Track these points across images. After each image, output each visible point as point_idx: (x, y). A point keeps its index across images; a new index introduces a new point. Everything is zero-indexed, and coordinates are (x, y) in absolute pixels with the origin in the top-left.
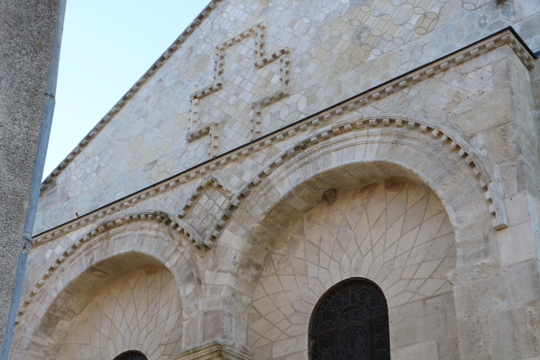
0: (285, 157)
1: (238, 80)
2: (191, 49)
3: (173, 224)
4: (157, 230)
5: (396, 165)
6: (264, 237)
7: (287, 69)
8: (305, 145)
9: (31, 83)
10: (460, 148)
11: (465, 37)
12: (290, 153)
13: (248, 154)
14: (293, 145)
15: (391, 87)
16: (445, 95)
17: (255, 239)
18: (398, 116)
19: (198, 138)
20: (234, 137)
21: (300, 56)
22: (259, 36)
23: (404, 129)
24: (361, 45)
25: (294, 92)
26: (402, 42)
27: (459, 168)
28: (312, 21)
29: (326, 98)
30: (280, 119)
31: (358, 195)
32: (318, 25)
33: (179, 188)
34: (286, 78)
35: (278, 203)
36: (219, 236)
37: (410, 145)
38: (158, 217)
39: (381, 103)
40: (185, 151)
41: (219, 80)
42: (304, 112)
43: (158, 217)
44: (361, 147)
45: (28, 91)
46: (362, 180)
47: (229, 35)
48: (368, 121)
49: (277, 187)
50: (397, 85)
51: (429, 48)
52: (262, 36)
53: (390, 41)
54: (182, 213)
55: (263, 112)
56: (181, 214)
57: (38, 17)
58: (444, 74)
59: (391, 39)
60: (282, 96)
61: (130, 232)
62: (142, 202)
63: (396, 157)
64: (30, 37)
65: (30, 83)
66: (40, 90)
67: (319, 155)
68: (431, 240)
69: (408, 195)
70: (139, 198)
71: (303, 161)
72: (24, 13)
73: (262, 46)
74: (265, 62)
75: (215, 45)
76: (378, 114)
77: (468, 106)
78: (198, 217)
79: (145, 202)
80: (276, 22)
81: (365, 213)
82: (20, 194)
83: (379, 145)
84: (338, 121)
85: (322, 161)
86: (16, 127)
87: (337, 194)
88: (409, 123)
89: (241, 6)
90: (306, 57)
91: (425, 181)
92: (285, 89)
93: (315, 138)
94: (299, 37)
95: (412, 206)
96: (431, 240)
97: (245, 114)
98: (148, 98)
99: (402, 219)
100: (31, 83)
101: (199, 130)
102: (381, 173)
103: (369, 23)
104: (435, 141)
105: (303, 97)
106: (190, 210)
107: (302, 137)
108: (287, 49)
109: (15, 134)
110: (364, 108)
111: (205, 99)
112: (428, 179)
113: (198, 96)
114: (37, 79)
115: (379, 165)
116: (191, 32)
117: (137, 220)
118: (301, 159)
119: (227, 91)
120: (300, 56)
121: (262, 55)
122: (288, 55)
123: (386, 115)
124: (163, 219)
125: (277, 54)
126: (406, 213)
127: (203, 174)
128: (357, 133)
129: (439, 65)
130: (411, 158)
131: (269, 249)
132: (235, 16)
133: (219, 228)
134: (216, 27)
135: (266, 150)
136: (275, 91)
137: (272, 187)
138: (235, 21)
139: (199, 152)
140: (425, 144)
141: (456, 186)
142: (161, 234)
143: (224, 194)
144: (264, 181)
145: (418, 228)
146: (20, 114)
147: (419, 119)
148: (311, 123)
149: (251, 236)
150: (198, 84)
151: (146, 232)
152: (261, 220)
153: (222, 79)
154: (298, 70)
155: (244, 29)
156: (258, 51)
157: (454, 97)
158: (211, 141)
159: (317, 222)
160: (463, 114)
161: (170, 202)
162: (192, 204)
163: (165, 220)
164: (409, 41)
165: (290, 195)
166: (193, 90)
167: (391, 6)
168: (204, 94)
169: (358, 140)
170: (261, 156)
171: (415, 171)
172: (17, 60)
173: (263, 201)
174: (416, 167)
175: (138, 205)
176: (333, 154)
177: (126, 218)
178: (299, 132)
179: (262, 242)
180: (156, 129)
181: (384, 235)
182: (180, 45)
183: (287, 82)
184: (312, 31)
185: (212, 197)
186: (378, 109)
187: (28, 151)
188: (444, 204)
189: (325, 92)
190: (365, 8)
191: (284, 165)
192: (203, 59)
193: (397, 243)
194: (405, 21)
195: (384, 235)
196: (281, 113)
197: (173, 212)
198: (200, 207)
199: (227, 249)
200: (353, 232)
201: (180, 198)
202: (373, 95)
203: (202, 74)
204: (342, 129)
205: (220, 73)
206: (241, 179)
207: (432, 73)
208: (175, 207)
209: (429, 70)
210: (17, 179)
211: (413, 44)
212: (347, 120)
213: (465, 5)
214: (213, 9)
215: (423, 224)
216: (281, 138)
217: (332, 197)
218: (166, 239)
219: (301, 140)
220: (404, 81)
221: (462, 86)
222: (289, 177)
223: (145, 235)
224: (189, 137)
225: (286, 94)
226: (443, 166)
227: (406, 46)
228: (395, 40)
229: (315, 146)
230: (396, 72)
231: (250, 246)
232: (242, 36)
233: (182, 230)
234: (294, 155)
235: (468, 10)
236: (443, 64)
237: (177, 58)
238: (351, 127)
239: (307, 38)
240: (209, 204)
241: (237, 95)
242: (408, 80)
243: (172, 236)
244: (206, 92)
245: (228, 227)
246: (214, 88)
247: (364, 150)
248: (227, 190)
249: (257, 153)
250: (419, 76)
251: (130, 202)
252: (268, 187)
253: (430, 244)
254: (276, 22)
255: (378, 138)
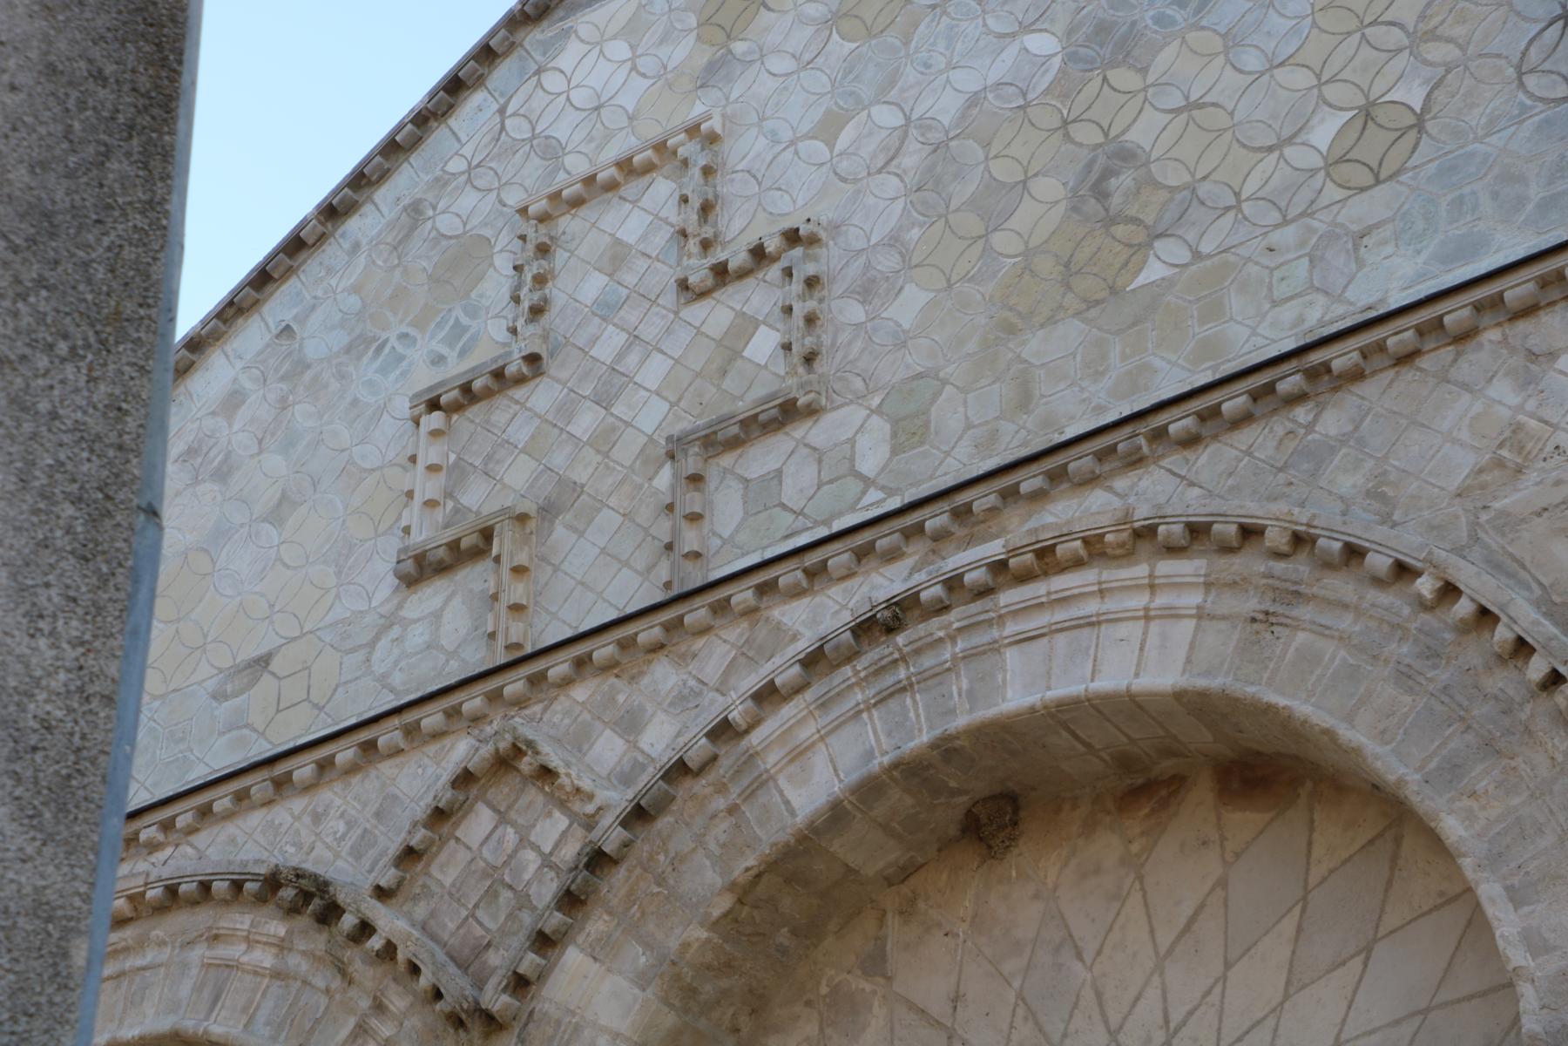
0: (815, 661)
1: (609, 344)
2: (415, 211)
3: (348, 921)
4: (282, 946)
5: (1269, 709)
6: (724, 983)
7: (811, 304)
8: (896, 617)
9: (90, 468)
10: (1533, 650)
11: (1530, 207)
12: (837, 648)
13: (662, 646)
14: (846, 617)
15: (1243, 398)
16: (1464, 435)
17: (690, 992)
18: (1277, 515)
19: (442, 569)
20: (598, 574)
21: (862, 260)
22: (696, 172)
23: (1299, 568)
24: (1110, 221)
25: (839, 400)
26: (1275, 217)
27: (1528, 731)
28: (908, 119)
29: (969, 426)
30: (783, 506)
31: (1108, 819)
32: (936, 136)
33: (373, 773)
34: (809, 341)
35: (787, 845)
36: (542, 976)
37: (1323, 631)
38: (288, 893)
39: (1204, 458)
40: (390, 621)
41: (530, 340)
42: (881, 481)
43: (288, 893)
44: (1123, 630)
45: (80, 499)
46: (1125, 762)
47: (569, 161)
48: (1151, 531)
49: (782, 782)
50: (1270, 389)
51: (1385, 242)
52: (707, 171)
53: (1228, 209)
54: (388, 878)
55: (713, 473)
56: (383, 883)
57: (109, 207)
58: (1458, 355)
59: (1232, 201)
60: (788, 413)
61: (165, 954)
62: (215, 829)
63: (1266, 675)
64: (81, 287)
65: (85, 468)
66: (121, 496)
67: (954, 657)
68: (1413, 1015)
69: (1312, 829)
70: (205, 812)
71: (888, 680)
72: (60, 195)
73: (706, 209)
74: (721, 273)
75: (514, 198)
76: (1193, 504)
77: (1558, 483)
78: (455, 895)
79: (230, 829)
80: (762, 119)
81: (1136, 897)
82: (60, 913)
83: (1197, 628)
84: (1031, 524)
85: (965, 684)
86: (42, 643)
87: (1022, 814)
88: (1321, 542)
89: (619, 50)
90: (887, 262)
91: (1391, 778)
92: (801, 386)
93: (937, 591)
94: (855, 181)
95: (1331, 871)
96: (1413, 1015)
97: (638, 480)
98: (233, 401)
99: (1288, 925)
100: (90, 468)
101: (448, 535)
102: (1199, 737)
103: (1139, 136)
104: (1425, 617)
105: (875, 419)
106: (419, 867)
107: (884, 584)
108: (811, 227)
109: (38, 673)
110: (1133, 475)
111: (475, 411)
112: (1402, 770)
113: (443, 400)
114: (111, 453)
115: (1196, 704)
116: (415, 143)
117: (194, 903)
118: (879, 671)
119: (565, 384)
120: (862, 260)
121: (706, 245)
122: (815, 250)
123: (1223, 509)
124: (311, 899)
125: (771, 246)
126: (1304, 898)
127: (477, 719)
128: (1105, 575)
129: (1441, 318)
130: (1329, 680)
131: (745, 1030)
132: (596, 82)
133: (544, 942)
134: (517, 128)
135: (735, 633)
136: (759, 391)
137: (763, 782)
138: (597, 108)
139: (445, 631)
140: (1386, 628)
141: (1516, 801)
142: (296, 962)
143: (562, 804)
144: (729, 756)
145: (1357, 963)
146: (53, 592)
147: (1361, 529)
148: (919, 529)
149: (677, 978)
150: (444, 351)
151: (235, 951)
152: (716, 913)
153: (545, 337)
154: (854, 312)
155: (633, 142)
156: (689, 230)
157: (1501, 446)
158: (499, 584)
159: (939, 925)
160: (1539, 515)
161: (332, 831)
162: (432, 842)
163: (316, 903)
164: (1303, 214)
165: (836, 815)
166: (424, 378)
167: (1229, 70)
168: (469, 394)
169: (1111, 605)
170: (716, 653)
171: (1346, 734)
172: (40, 382)
173: (723, 838)
174: (1349, 719)
175: (201, 839)
176: (1011, 656)
177: (150, 894)
178: (870, 563)
179: (718, 1002)
180: (267, 526)
181: (1217, 990)
182: (366, 192)
183: (809, 359)
184: (913, 158)
185: (513, 815)
186: (1192, 484)
187: (83, 737)
188: (1470, 874)
189: (965, 402)
190: (1123, 78)
191: (809, 695)
192: (467, 254)
193: (1271, 1022)
194: (1286, 133)
195: (1217, 990)
196: (788, 481)
197: (352, 874)
198: (463, 856)
199: (577, 1029)
200: (1090, 969)
201: (378, 815)
202: (1172, 428)
203: (458, 312)
204: (1046, 560)
205: (537, 311)
206: (634, 746)
207: (1410, 348)
208: (357, 853)
209: (1398, 336)
210: (48, 850)
211: (1319, 224)
212: (1068, 522)
213: (1531, 81)
214: (506, 54)
215: (1380, 950)
216: (797, 585)
217: (1002, 827)
218: (319, 982)
219: (881, 595)
220: (1298, 377)
221: (1531, 405)
222: (831, 740)
223: (230, 966)
224: (409, 566)
225: (809, 405)
226: (1462, 719)
227: (1289, 234)
228: (1245, 206)
229: (936, 622)
230: (1254, 333)
231: (670, 1020)
232: (627, 167)
233: (390, 950)
234: (851, 656)
235: (1541, 99)
236: (1456, 313)
237: (356, 246)
238: (1083, 552)
239: (892, 185)
240: (500, 841)
241: (604, 401)
242: (1313, 374)
243: (342, 971)
244: (477, 385)
245: (580, 939)
246: (511, 370)
247: (1137, 645)
248: (578, 790)
249: (700, 642)
250: (1356, 356)
251: (167, 826)
252: (745, 782)
253: (1407, 1030)
254: (762, 119)
255: (1193, 599)
